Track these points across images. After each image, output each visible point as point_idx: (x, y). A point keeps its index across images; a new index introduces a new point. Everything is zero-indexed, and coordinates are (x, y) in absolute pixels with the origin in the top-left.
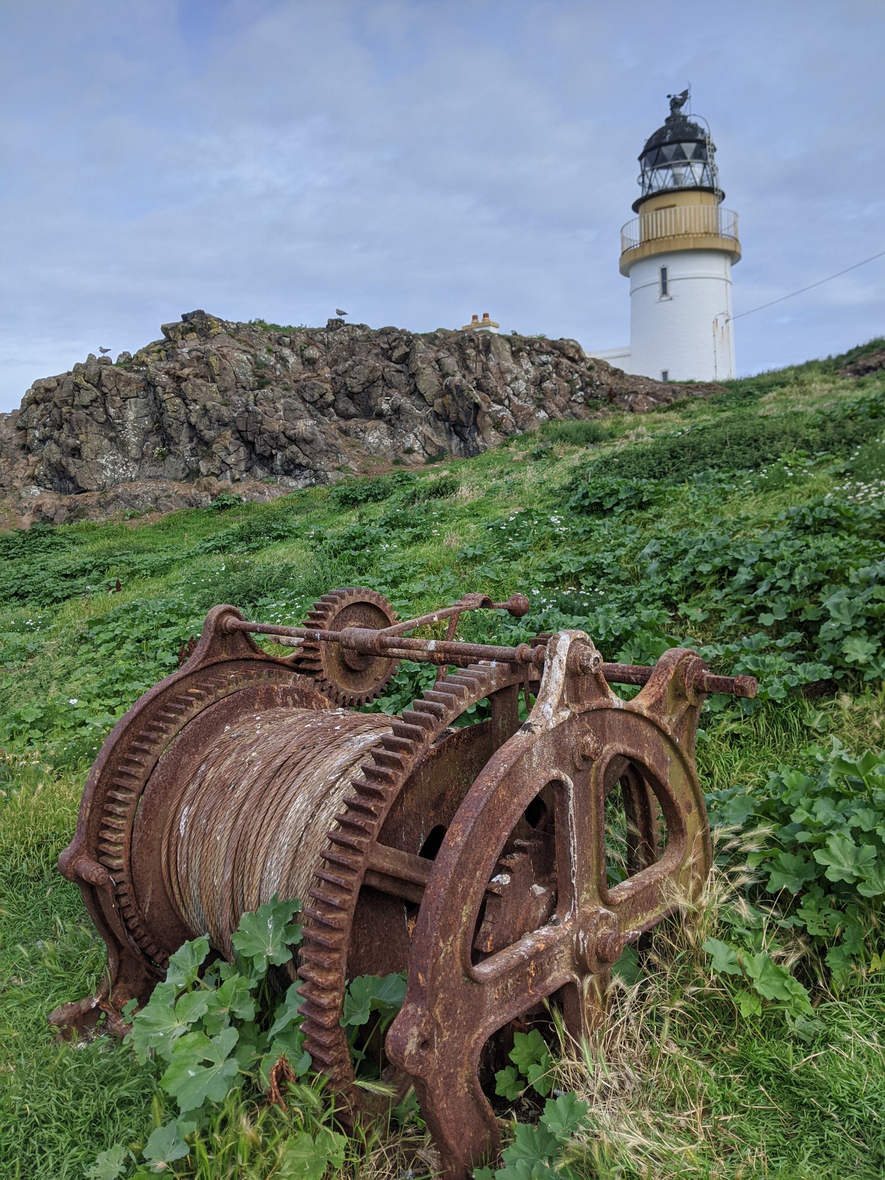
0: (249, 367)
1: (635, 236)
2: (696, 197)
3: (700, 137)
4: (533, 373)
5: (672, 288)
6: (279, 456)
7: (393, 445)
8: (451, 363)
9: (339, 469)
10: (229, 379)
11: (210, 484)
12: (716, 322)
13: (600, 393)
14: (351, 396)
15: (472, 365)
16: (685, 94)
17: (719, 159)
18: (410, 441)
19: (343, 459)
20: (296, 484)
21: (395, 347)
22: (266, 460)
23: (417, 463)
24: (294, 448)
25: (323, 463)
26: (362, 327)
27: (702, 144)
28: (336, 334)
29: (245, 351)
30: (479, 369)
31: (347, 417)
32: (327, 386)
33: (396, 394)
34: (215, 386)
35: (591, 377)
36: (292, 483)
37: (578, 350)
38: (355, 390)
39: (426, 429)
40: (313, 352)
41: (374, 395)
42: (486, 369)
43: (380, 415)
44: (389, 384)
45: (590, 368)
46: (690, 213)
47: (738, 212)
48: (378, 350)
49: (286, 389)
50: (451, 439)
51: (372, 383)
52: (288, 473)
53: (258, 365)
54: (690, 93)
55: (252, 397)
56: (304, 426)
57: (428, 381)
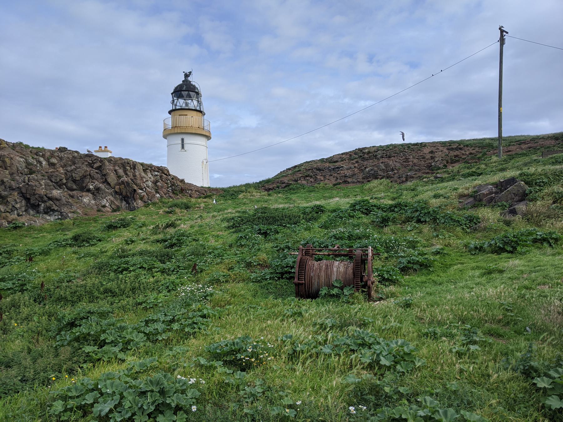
0: (24, 165)
1: (170, 124)
2: (195, 113)
3: (196, 91)
4: (152, 179)
5: (185, 146)
6: (43, 205)
7: (96, 203)
8: (121, 172)
9: (73, 212)
10: (14, 169)
11: (7, 216)
12: (203, 162)
13: (177, 189)
14: (74, 181)
15: (129, 173)
16: (190, 73)
17: (203, 99)
18: (104, 202)
19: (74, 208)
20: (51, 218)
21: (95, 163)
22: (35, 207)
23: (108, 212)
24: (51, 202)
25: (65, 210)
26: (76, 152)
27: (198, 94)
28: (65, 154)
29: (21, 157)
30: (132, 175)
31: (72, 190)
32: (63, 176)
33: (96, 183)
34: (8, 171)
35: (174, 182)
36: (48, 218)
37: (168, 171)
38: (77, 179)
39: (110, 197)
40: (54, 160)
41: (85, 182)
42: (135, 176)
43: (89, 190)
44: (92, 178)
45: (173, 179)
46: (191, 119)
47: (212, 121)
48: (87, 163)
49: (43, 176)
50: (122, 202)
51: (85, 176)
52: (46, 213)
53: (28, 164)
54: (193, 73)
55: (27, 178)
56: (56, 193)
57: (112, 178)
